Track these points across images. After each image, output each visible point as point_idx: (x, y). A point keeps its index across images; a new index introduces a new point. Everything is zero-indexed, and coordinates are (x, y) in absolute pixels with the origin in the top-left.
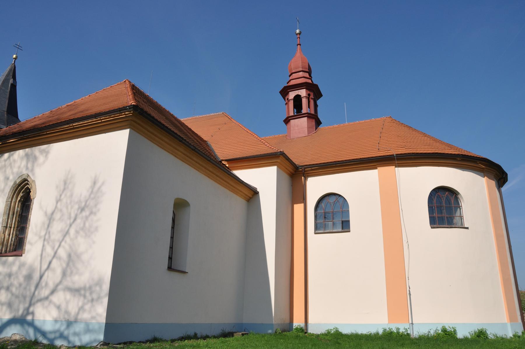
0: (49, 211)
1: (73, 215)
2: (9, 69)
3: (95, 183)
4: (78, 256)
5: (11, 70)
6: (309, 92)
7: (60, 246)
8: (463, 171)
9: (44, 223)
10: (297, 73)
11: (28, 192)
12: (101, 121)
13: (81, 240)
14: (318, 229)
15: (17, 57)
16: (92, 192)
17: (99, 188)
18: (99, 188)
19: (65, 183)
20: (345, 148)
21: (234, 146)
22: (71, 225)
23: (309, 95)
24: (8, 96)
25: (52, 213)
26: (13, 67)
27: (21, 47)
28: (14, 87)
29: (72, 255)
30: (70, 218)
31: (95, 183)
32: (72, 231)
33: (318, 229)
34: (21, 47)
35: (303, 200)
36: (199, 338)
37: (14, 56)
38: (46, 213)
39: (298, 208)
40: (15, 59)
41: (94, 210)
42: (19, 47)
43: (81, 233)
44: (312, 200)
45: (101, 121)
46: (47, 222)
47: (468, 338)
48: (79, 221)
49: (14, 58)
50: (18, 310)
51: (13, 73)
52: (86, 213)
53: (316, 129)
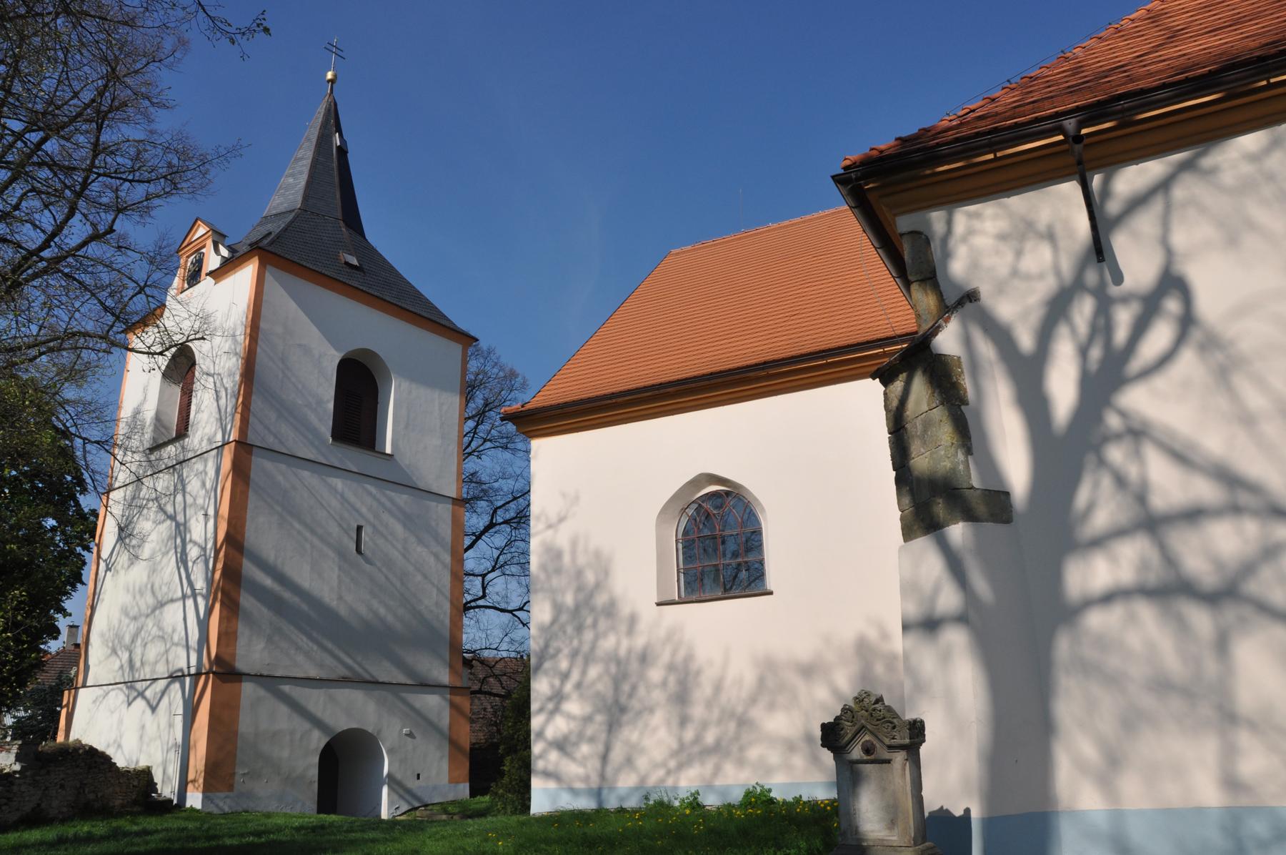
2: (323, 110)
5: (328, 111)
12: (1272, 80)
15: (335, 76)
20: (823, 276)
21: (627, 351)
24: (337, 180)
26: (332, 104)
27: (342, 51)
34: (342, 51)
36: (914, 282)
37: (330, 75)
40: (332, 81)
42: (338, 52)
45: (1272, 80)
47: (939, 392)
49: (329, 81)
50: (512, 761)
51: (333, 121)
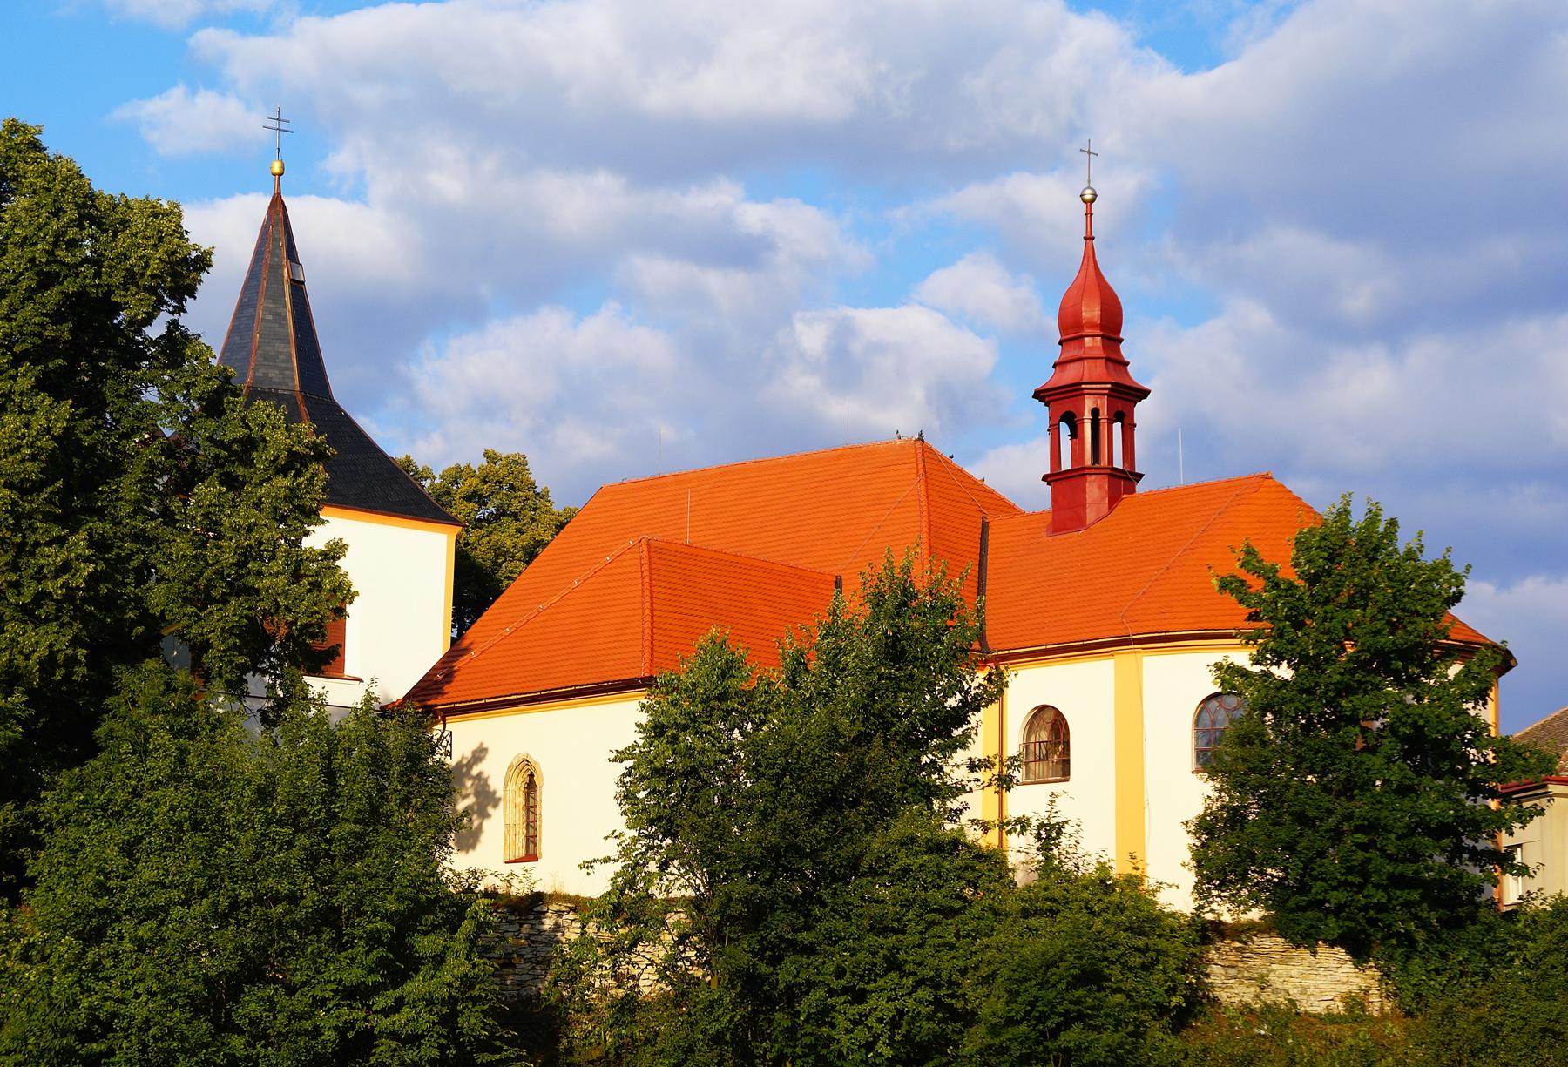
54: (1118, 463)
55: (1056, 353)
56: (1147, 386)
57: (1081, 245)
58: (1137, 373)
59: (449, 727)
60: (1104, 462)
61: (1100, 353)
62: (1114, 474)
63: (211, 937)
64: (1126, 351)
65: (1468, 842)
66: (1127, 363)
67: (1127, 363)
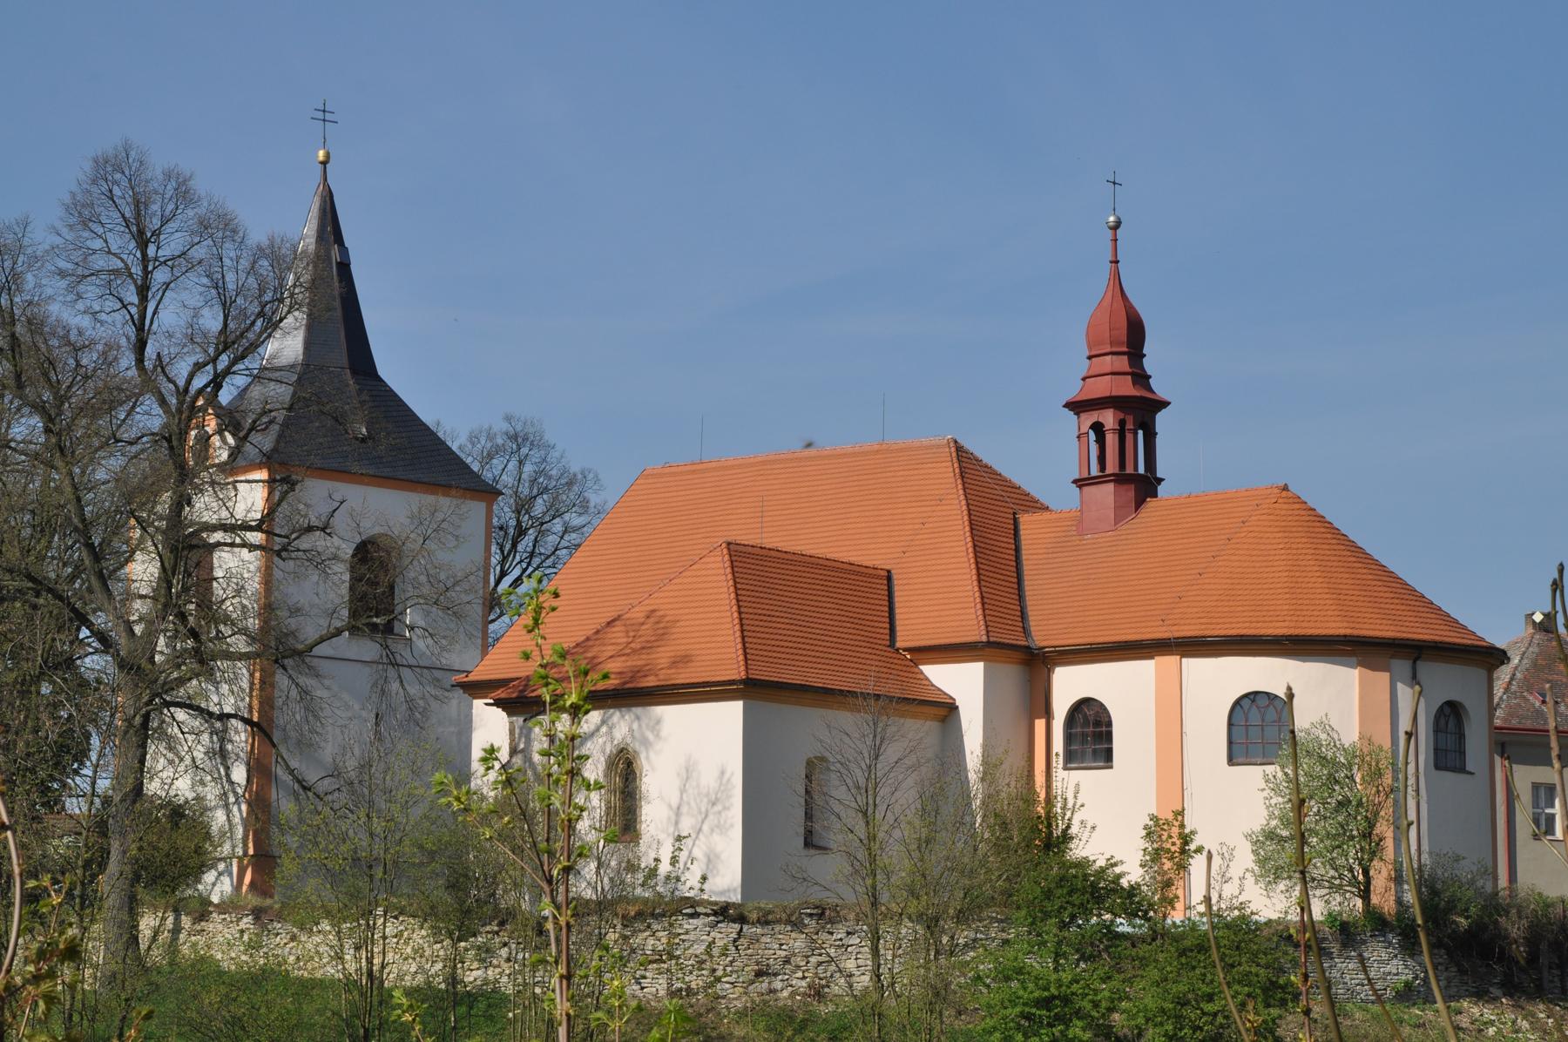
0: (675, 805)
1: (703, 810)
3: (723, 773)
4: (717, 856)
6: (1121, 416)
7: (694, 844)
8: (1304, 661)
9: (669, 818)
10: (1101, 358)
11: (629, 764)
13: (716, 837)
14: (1071, 759)
15: (328, 156)
16: (721, 784)
17: (729, 780)
18: (729, 780)
19: (687, 771)
22: (703, 822)
23: (1122, 423)
25: (678, 808)
28: (344, 268)
29: (712, 856)
30: (700, 813)
31: (723, 773)
32: (705, 828)
33: (1071, 759)
35: (1048, 714)
37: (321, 154)
38: (670, 806)
39: (1040, 724)
40: (324, 163)
41: (727, 805)
43: (717, 830)
44: (1060, 709)
46: (673, 818)
48: (711, 817)
52: (718, 807)
53: (1136, 510)
54: (1141, 470)
55: (1083, 367)
56: (1169, 400)
57: (1107, 267)
58: (1161, 387)
59: (242, 669)
60: (1129, 470)
61: (1128, 369)
62: (1134, 479)
63: (1355, 833)
64: (1149, 365)
65: (63, 392)
66: (1150, 377)
67: (1150, 377)
